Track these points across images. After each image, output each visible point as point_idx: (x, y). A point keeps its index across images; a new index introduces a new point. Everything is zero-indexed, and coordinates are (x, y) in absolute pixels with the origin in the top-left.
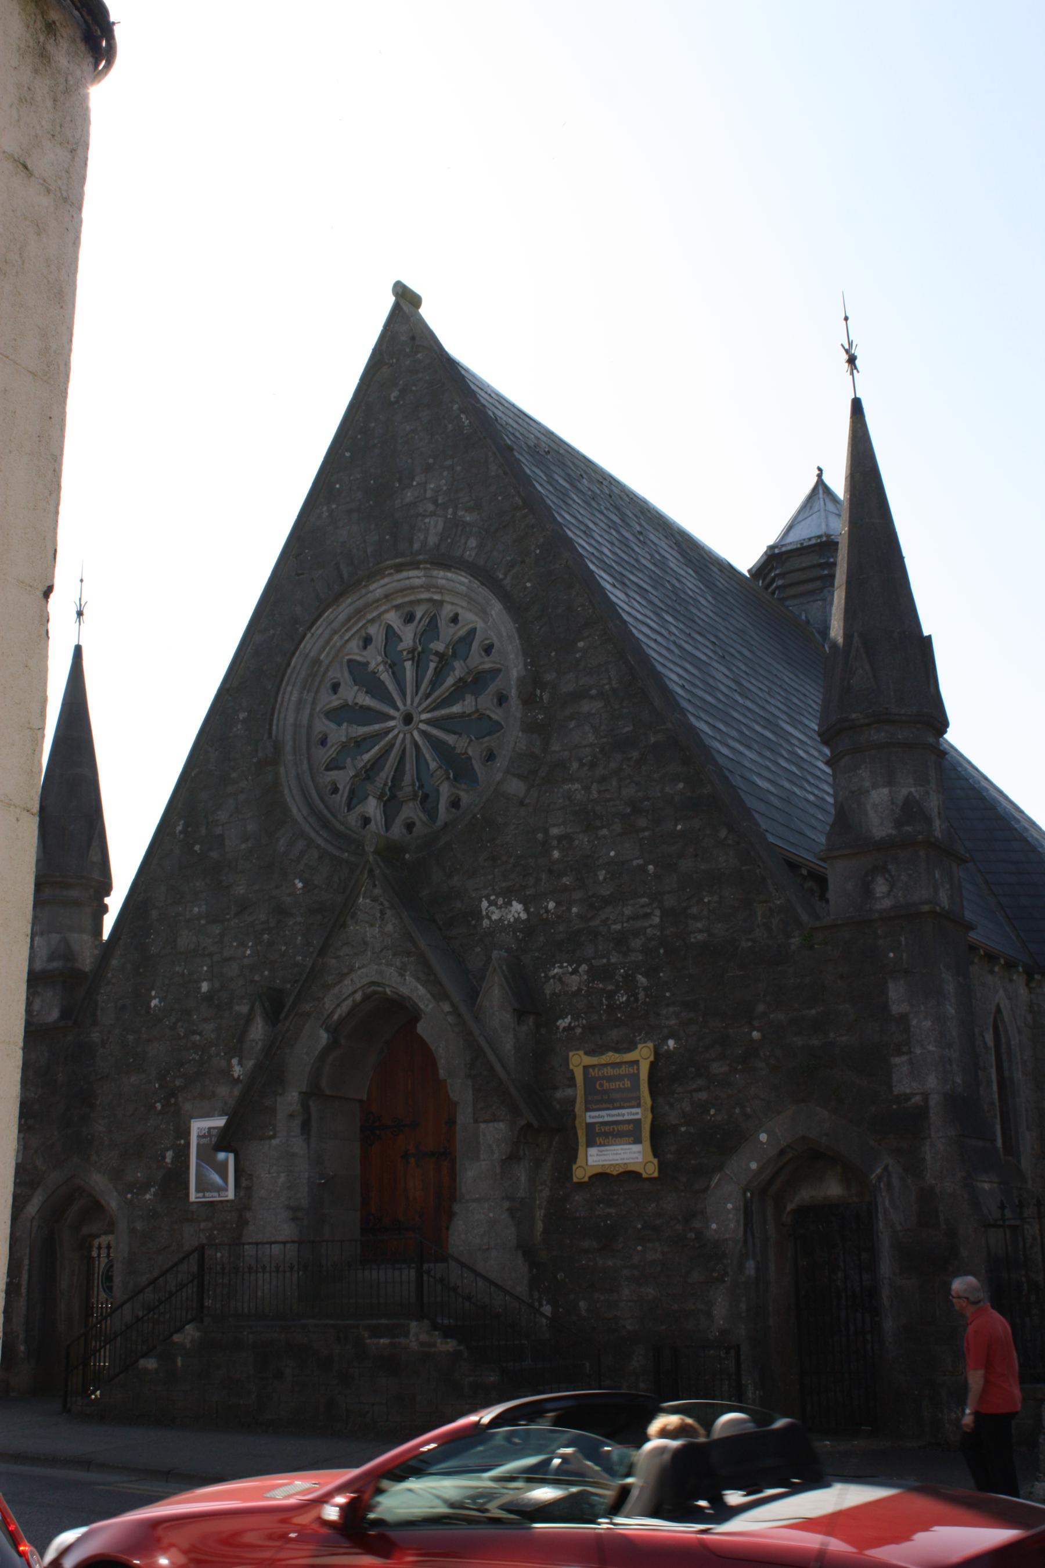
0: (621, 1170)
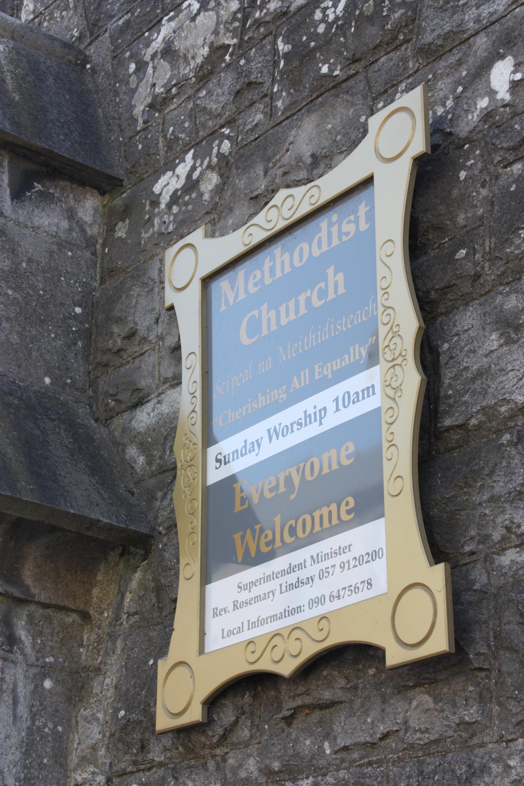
0: (311, 649)
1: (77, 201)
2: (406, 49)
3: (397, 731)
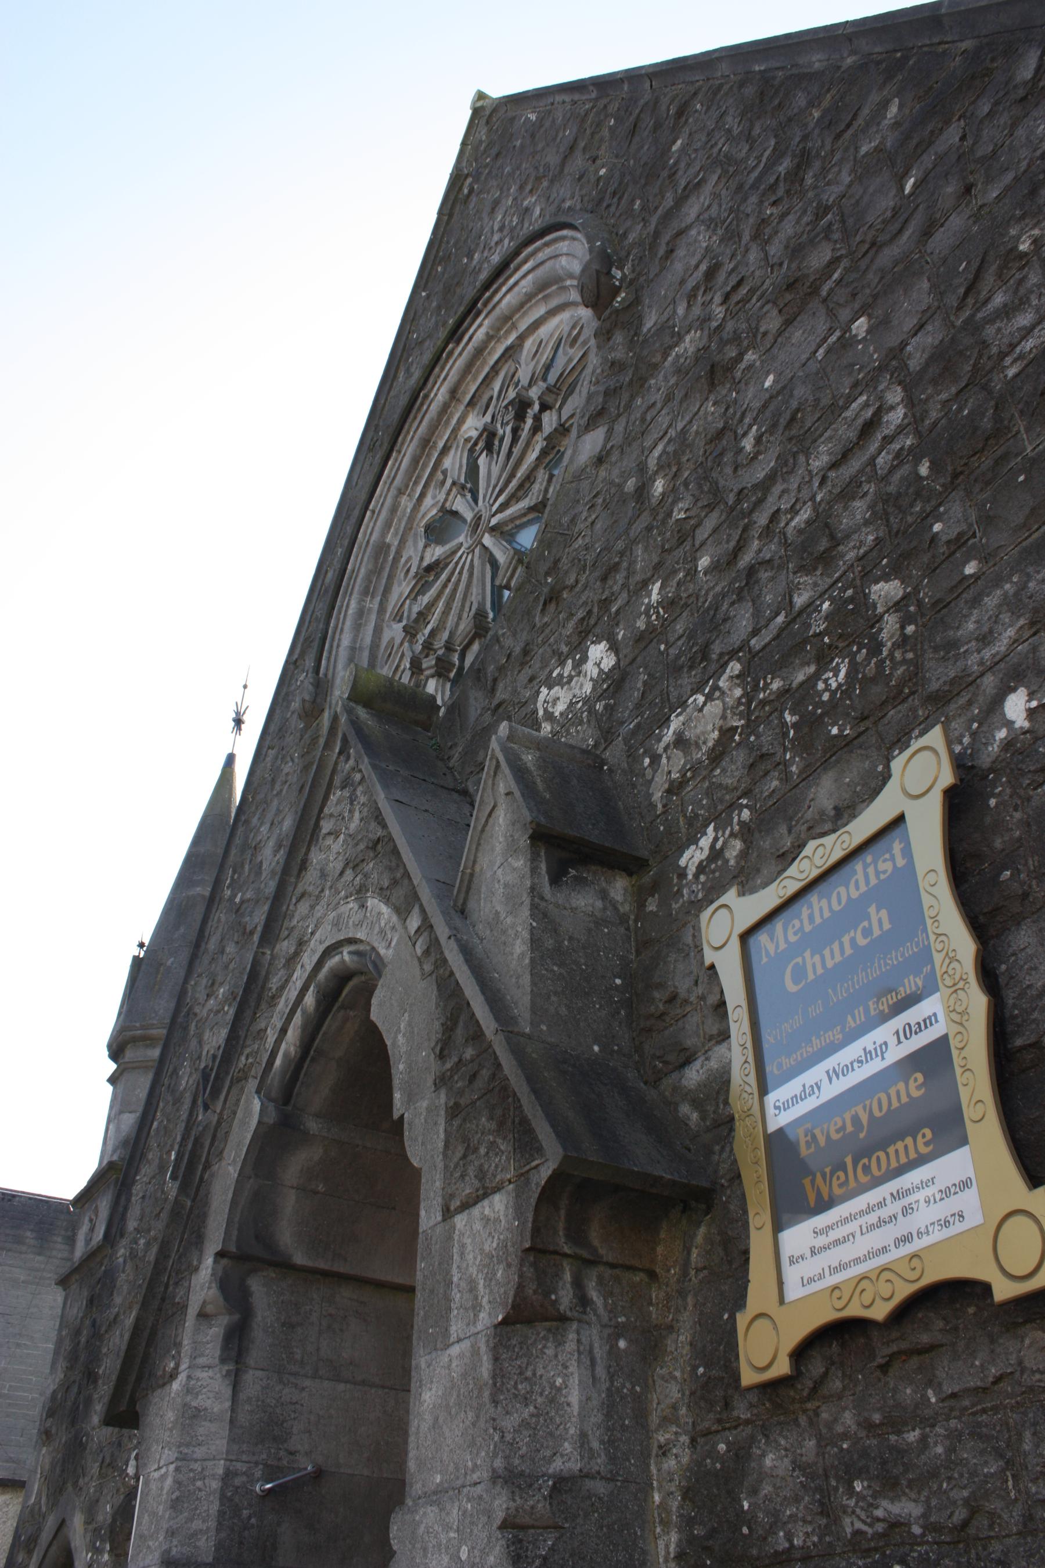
0: (904, 1291)
1: (609, 882)
2: (913, 700)
3: (1012, 1373)
